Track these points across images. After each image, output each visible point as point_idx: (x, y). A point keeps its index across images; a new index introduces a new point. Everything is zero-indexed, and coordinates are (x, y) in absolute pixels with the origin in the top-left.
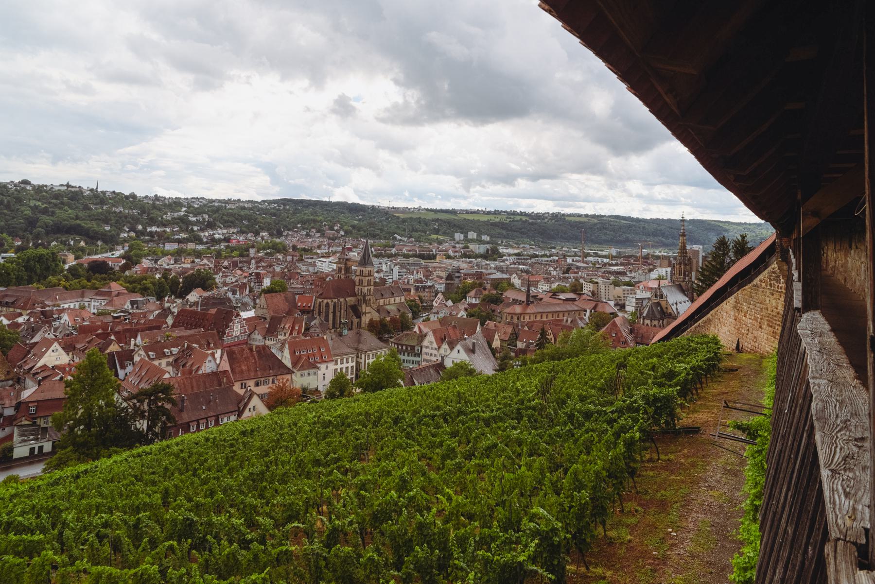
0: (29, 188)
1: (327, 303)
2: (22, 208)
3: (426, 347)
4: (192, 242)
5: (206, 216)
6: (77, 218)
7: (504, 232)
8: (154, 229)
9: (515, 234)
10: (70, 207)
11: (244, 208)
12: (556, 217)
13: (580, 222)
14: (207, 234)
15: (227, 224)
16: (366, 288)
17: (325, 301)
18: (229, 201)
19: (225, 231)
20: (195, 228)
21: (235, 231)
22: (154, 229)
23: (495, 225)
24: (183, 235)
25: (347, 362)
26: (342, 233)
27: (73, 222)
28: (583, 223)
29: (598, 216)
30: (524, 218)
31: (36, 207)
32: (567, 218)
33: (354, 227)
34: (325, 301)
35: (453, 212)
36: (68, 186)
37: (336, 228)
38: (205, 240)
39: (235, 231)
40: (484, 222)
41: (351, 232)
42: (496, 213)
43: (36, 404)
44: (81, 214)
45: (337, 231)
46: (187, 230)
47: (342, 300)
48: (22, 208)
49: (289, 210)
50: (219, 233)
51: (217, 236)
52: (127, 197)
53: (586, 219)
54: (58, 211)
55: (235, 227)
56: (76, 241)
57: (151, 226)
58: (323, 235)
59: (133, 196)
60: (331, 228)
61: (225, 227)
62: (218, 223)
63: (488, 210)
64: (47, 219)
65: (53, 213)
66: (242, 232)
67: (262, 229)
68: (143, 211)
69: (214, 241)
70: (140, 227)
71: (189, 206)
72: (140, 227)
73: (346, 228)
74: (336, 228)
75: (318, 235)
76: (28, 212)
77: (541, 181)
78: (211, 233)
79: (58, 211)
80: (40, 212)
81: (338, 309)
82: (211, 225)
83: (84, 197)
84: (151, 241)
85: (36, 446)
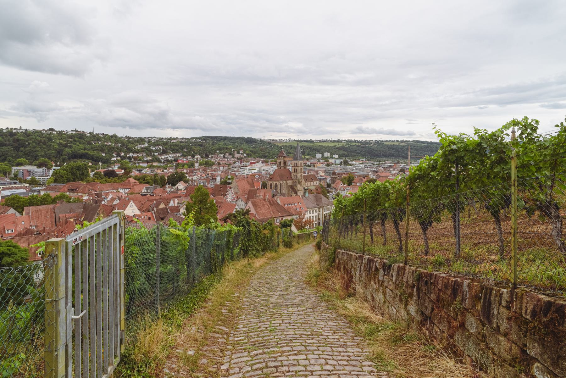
0: (54, 133)
1: (276, 184)
2: (53, 144)
5: (161, 147)
6: (85, 149)
7: (346, 153)
8: (131, 155)
10: (80, 143)
11: (181, 142)
12: (377, 142)
13: (394, 145)
14: (163, 157)
15: (174, 151)
17: (275, 183)
18: (171, 139)
20: (156, 154)
21: (180, 155)
22: (131, 155)
23: (339, 148)
26: (245, 155)
28: (396, 145)
30: (357, 144)
32: (385, 143)
33: (252, 151)
34: (275, 183)
35: (311, 141)
36: (76, 131)
37: (241, 152)
39: (180, 155)
40: (332, 147)
42: (339, 141)
44: (87, 147)
45: (242, 154)
47: (284, 182)
49: (209, 143)
50: (171, 157)
51: (170, 159)
52: (112, 137)
53: (397, 144)
55: (179, 153)
57: (129, 153)
58: (233, 157)
59: (115, 136)
60: (238, 153)
61: (174, 153)
62: (169, 151)
64: (67, 150)
65: (71, 147)
66: (184, 156)
67: (196, 154)
68: (123, 145)
70: (123, 154)
71: (149, 141)
72: (123, 154)
73: (247, 152)
74: (241, 152)
75: (230, 157)
76: (56, 146)
77: (337, 140)
78: (166, 156)
80: (63, 146)
82: (165, 152)
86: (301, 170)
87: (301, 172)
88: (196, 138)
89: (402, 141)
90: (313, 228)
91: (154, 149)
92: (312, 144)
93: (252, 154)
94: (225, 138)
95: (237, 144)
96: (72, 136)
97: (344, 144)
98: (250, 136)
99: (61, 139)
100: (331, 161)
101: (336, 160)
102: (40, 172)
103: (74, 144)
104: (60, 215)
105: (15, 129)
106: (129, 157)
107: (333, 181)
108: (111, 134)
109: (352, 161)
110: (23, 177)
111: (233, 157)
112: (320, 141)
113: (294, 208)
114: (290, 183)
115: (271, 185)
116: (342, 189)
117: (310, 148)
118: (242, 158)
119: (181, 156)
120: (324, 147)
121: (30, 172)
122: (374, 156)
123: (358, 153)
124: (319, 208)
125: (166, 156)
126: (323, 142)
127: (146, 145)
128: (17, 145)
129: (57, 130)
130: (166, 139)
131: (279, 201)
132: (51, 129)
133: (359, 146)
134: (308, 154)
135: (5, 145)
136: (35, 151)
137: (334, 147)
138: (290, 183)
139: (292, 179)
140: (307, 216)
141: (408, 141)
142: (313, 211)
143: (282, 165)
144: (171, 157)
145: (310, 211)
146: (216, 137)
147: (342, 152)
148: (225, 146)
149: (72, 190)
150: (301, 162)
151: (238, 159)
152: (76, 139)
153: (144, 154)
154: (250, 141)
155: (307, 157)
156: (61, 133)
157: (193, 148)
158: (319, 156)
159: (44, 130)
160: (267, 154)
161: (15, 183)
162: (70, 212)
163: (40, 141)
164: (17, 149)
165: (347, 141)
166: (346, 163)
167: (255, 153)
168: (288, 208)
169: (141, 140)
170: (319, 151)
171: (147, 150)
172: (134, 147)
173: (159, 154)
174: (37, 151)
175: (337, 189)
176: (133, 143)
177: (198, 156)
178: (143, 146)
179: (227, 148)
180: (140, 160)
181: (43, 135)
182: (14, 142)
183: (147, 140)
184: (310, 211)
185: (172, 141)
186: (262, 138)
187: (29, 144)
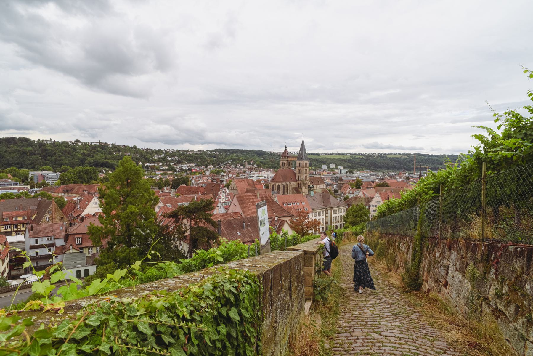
0: (79, 144)
1: (279, 185)
2: (77, 154)
3: (373, 206)
4: (170, 170)
5: (177, 158)
6: (106, 158)
7: (350, 165)
8: (148, 164)
9: (357, 165)
10: (102, 153)
11: (197, 154)
12: (380, 155)
13: (396, 158)
14: (178, 167)
15: (189, 161)
16: (304, 175)
17: (277, 184)
18: (188, 151)
19: (188, 165)
20: (171, 164)
21: (194, 165)
22: (148, 164)
23: (343, 161)
24: (165, 167)
25: (319, 215)
26: (255, 166)
27: (104, 160)
28: (398, 158)
29: (407, 154)
30: (361, 157)
31: (84, 153)
32: (387, 156)
33: (262, 163)
34: (277, 184)
35: (318, 154)
36: (100, 142)
37: (251, 163)
38: (178, 170)
39: (194, 165)
40: (337, 159)
41: (261, 166)
42: (343, 154)
43: (81, 236)
44: (108, 156)
45: (252, 165)
46: (167, 165)
47: (288, 183)
48: (77, 154)
49: (222, 155)
50: (185, 166)
51: (184, 168)
52: (131, 148)
53: (400, 156)
54: (95, 155)
55: (194, 163)
56: (106, 171)
57: (146, 162)
58: (244, 167)
59: (135, 147)
60: (249, 163)
61: (188, 163)
62: (184, 161)
63: (338, 153)
65: (93, 156)
66: (198, 166)
67: (209, 164)
68: (141, 155)
69: (182, 170)
72: (141, 163)
73: (257, 163)
74: (251, 163)
75: (242, 167)
76: (80, 156)
77: (341, 153)
78: (181, 166)
79: (95, 155)
80: (86, 156)
81: (285, 189)
82: (180, 162)
83: (109, 148)
84: (147, 170)
85: (82, 269)
86: (306, 171)
87: (306, 173)
88: (211, 151)
89: (404, 154)
90: (320, 233)
91: (170, 159)
92: (318, 157)
93: (262, 165)
94: (237, 151)
95: (248, 156)
96: (95, 147)
97: (348, 157)
98: (260, 149)
99: (85, 150)
100: (336, 171)
101: (342, 172)
102: (53, 176)
103: (96, 154)
104: (4, 213)
105: (46, 140)
106: (147, 166)
107: (340, 187)
108: (131, 145)
109: (357, 171)
110: (38, 181)
111: (244, 167)
112: (326, 154)
113: (296, 208)
114: (294, 184)
115: (273, 187)
116: (351, 192)
117: (317, 160)
118: (252, 169)
119: (195, 166)
120: (330, 159)
121: (44, 176)
122: (378, 168)
123: (362, 165)
124: (327, 210)
125: (181, 166)
126: (329, 155)
127: (163, 156)
128: (44, 154)
129: (83, 142)
130: (182, 151)
131: (276, 200)
132: (77, 141)
133: (363, 158)
134: (315, 166)
135: (35, 154)
136: (60, 160)
137: (339, 160)
138: (294, 184)
139: (297, 181)
140: (312, 217)
141: (410, 154)
142: (319, 213)
143: (286, 166)
144: (185, 166)
145: (316, 213)
146: (229, 150)
147: (347, 164)
148: (237, 158)
149: (67, 191)
150: (306, 162)
151: (248, 169)
152: (99, 149)
153: (161, 164)
154: (260, 153)
155: (313, 168)
156: (85, 144)
157: (207, 159)
158: (325, 167)
159: (71, 142)
160: (276, 165)
161: (16, 184)
162: (19, 209)
163: (66, 151)
164: (45, 158)
165: (351, 154)
166: (351, 172)
167: (265, 164)
168: (288, 208)
169: (159, 152)
170: (324, 163)
171: (164, 160)
172: (152, 157)
173: (175, 164)
174: (62, 160)
175: (345, 194)
176: (151, 154)
177: (211, 166)
178: (160, 156)
179: (239, 160)
180: (157, 169)
181: (69, 145)
182: (42, 151)
183: (164, 151)
184: (316, 213)
185: (188, 153)
186: (272, 151)
187: (55, 154)
